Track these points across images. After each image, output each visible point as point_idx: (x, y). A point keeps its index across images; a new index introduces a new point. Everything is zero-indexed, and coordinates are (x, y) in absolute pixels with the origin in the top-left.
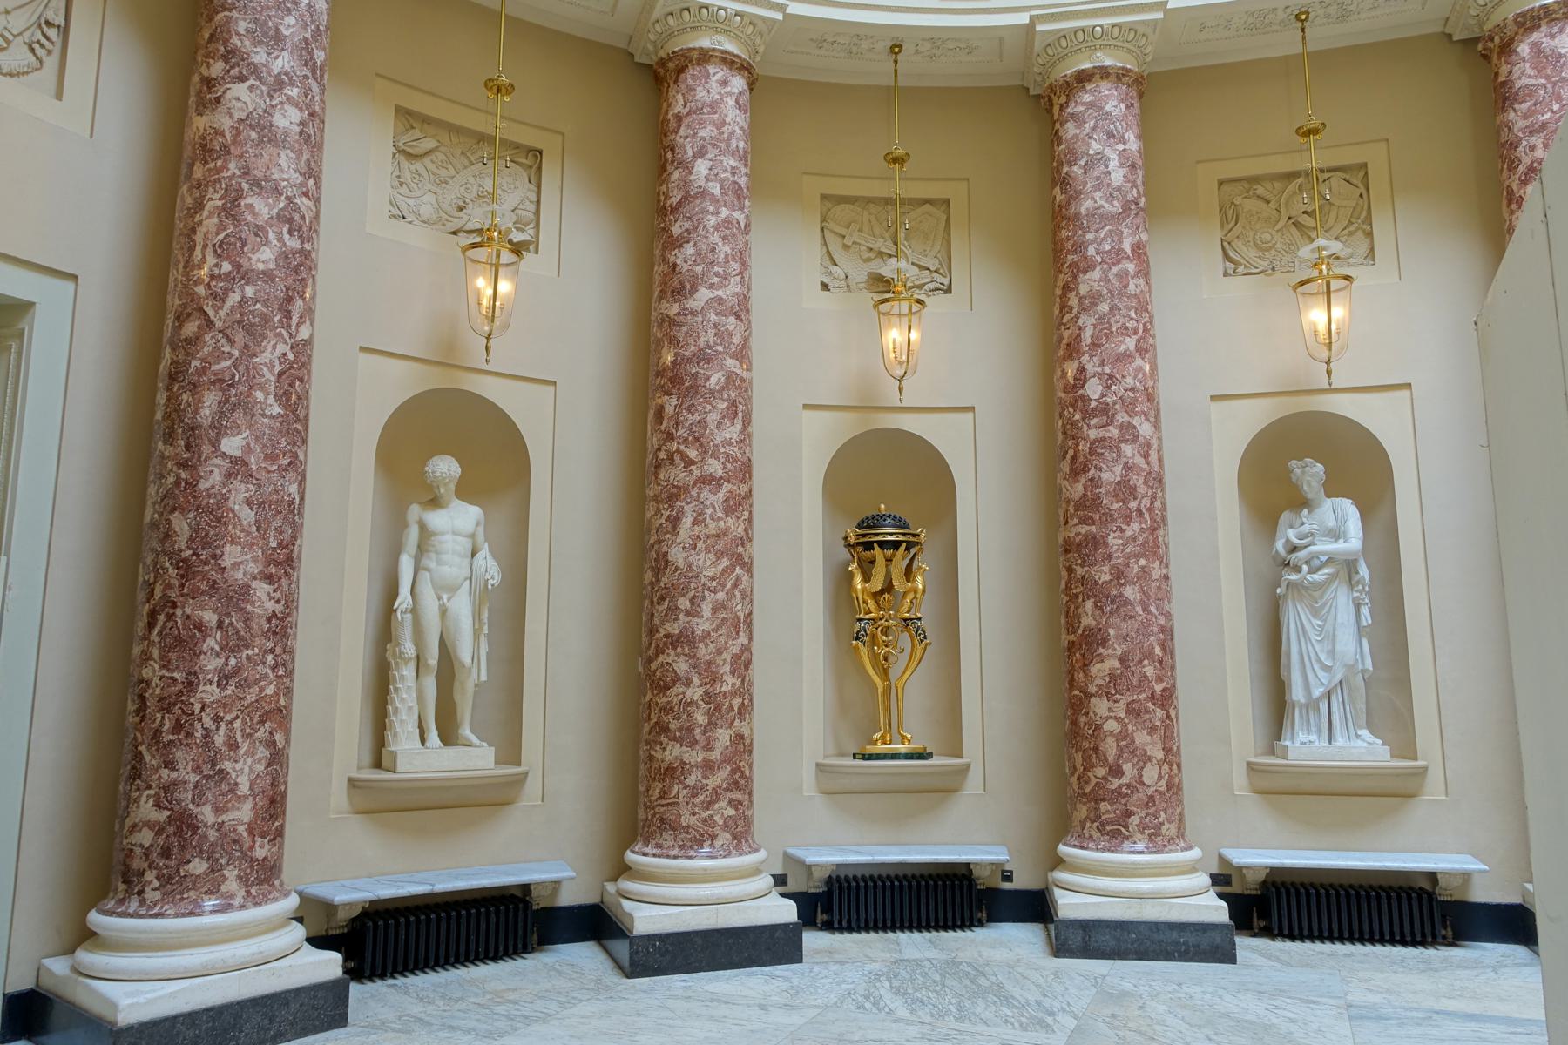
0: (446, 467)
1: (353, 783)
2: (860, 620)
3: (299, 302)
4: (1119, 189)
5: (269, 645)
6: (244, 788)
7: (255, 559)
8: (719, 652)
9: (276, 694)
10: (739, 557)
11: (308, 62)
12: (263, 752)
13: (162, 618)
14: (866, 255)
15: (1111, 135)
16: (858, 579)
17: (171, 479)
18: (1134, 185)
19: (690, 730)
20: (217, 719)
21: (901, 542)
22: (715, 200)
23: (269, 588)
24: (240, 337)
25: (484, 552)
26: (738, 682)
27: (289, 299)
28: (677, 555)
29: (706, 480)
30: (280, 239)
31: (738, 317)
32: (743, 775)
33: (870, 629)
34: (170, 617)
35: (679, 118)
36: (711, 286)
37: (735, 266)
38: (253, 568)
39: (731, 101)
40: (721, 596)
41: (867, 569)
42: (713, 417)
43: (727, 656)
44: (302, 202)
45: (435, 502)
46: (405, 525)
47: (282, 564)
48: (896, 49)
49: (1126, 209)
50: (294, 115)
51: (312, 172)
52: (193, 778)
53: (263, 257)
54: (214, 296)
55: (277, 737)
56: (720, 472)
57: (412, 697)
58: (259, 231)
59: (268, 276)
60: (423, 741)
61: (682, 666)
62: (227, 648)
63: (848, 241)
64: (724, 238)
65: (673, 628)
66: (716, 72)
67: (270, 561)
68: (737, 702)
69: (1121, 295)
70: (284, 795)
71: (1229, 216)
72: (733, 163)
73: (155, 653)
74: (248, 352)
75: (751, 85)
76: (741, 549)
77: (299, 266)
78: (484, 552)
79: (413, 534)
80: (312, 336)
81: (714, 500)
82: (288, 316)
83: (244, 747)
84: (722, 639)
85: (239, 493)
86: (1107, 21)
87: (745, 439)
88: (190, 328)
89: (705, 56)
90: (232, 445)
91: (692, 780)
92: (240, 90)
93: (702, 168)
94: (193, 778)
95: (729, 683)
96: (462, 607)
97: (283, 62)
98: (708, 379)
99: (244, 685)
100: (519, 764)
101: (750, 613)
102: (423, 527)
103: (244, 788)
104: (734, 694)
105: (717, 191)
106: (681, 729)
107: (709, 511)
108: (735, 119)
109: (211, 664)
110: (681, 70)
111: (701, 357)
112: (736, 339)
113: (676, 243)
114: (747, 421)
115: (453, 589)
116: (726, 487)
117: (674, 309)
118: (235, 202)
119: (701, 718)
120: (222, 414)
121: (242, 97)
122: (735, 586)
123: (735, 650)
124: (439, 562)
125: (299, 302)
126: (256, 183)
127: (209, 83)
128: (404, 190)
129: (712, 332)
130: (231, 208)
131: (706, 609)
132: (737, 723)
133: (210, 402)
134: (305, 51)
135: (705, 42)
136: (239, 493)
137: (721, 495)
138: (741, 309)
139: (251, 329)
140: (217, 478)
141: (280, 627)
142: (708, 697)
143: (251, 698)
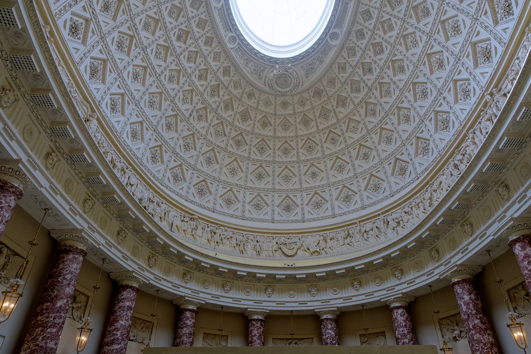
4: (465, 312)
15: (460, 298)
18: (469, 309)
22: (400, 339)
39: (399, 316)
49: (468, 316)
66: (395, 311)
69: (473, 340)
71: (512, 299)
72: (402, 329)
86: (393, 297)
105: (400, 337)
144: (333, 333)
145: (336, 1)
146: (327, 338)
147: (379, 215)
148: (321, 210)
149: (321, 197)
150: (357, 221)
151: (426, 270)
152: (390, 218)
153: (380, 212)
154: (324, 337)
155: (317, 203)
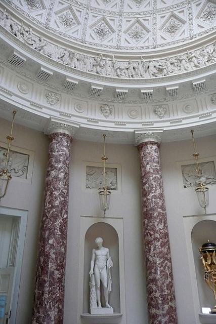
0: (99, 240)
1: (82, 317)
2: (206, 272)
3: (64, 210)
5: (58, 285)
6: (53, 318)
7: (55, 266)
8: (163, 284)
9: (60, 296)
10: (166, 258)
11: (66, 164)
12: (57, 310)
13: (38, 279)
14: (195, 177)
16: (204, 261)
17: (40, 249)
19: (157, 305)
20: (48, 302)
21: (213, 251)
22: (151, 173)
23: (57, 272)
24: (52, 219)
25: (110, 259)
26: (169, 292)
27: (62, 210)
28: (150, 258)
29: (156, 239)
30: (60, 199)
31: (160, 199)
32: (173, 318)
33: (209, 275)
34: (40, 279)
35: (142, 157)
36: (153, 193)
37: (158, 187)
38: (55, 268)
39: (153, 151)
40: (162, 268)
41: (206, 258)
42: (156, 223)
43: (165, 284)
44: (64, 191)
45: (98, 248)
46: (92, 254)
47: (61, 266)
48: (192, 131)
50: (63, 174)
51: (67, 184)
52: (43, 315)
53: (57, 203)
54: (48, 212)
55: (60, 306)
56: (159, 237)
57: (95, 295)
58: (56, 198)
59: (58, 206)
60: (98, 306)
61: (154, 287)
62: (50, 286)
63: (190, 175)
64: (155, 181)
65: (151, 277)
66: (149, 146)
67: (58, 266)
68: (169, 297)
70: (62, 320)
73: (37, 287)
74: (54, 222)
75: (159, 147)
76: (166, 256)
77: (64, 204)
78: (110, 259)
79: (94, 255)
80: (67, 217)
81: (158, 244)
82: (62, 214)
83: (53, 308)
84: (163, 280)
85: (52, 251)
86: (151, 132)
87: (166, 227)
88: (44, 219)
89: (146, 143)
90: (51, 242)
91: (159, 319)
92: (53, 172)
93: (148, 167)
94: (43, 315)
95: (166, 292)
96: (105, 273)
97: (60, 165)
98: (154, 214)
99: (53, 294)
100: (120, 313)
101: (171, 272)
102: (95, 254)
103: (53, 318)
104: (168, 295)
105: (152, 171)
106: (155, 305)
107: (157, 247)
108: (155, 155)
109: (47, 289)
110: (142, 147)
111: (152, 209)
112: (160, 204)
113: (144, 184)
114: (165, 223)
115: (102, 269)
116: (161, 240)
117: (145, 199)
118: (52, 193)
119: (160, 302)
120: (49, 235)
121: (53, 173)
122: (166, 265)
123: (167, 283)
124: (99, 262)
125: (64, 210)
126: (55, 189)
127: (48, 172)
128: (89, 182)
129: (154, 203)
130: (51, 195)
131: (159, 273)
132: (170, 303)
133: (47, 232)
134: (65, 163)
135: (146, 140)
136: (52, 251)
137: (160, 242)
138: (161, 196)
139: (55, 217)
140: (48, 249)
141: (61, 280)
142: (162, 296)
143: (54, 297)
144: (68, 153)
145: (2, 8)
146: (60, 155)
147: (140, 58)
148: (69, 28)
149: (74, 15)
150: (113, 55)
151: (201, 113)
152: (151, 64)
153: (142, 56)
154: (56, 154)
155: (68, 20)
